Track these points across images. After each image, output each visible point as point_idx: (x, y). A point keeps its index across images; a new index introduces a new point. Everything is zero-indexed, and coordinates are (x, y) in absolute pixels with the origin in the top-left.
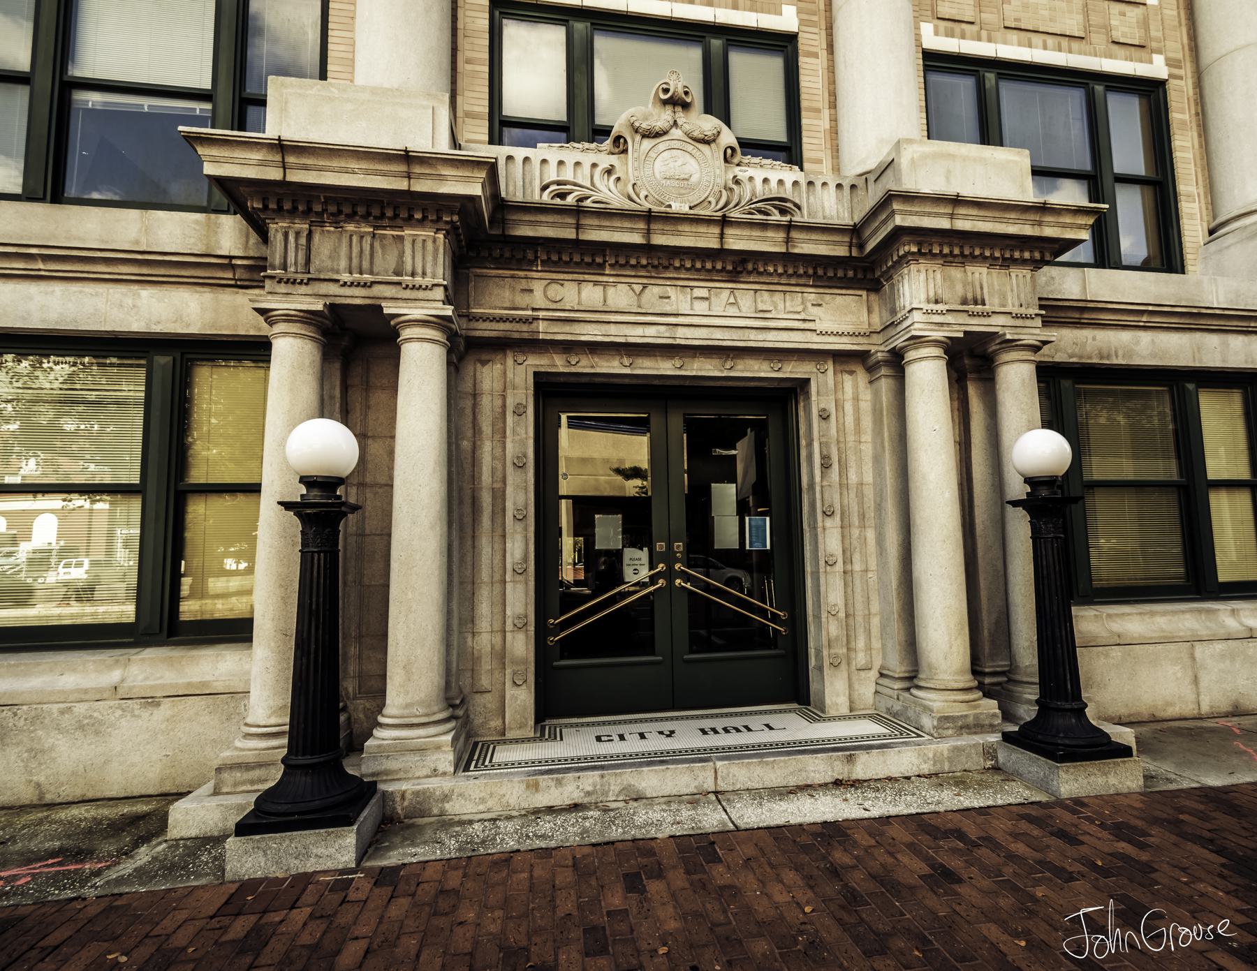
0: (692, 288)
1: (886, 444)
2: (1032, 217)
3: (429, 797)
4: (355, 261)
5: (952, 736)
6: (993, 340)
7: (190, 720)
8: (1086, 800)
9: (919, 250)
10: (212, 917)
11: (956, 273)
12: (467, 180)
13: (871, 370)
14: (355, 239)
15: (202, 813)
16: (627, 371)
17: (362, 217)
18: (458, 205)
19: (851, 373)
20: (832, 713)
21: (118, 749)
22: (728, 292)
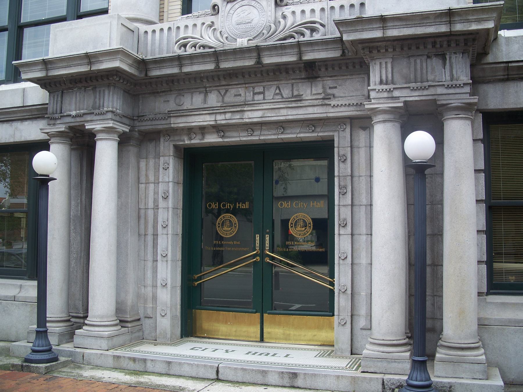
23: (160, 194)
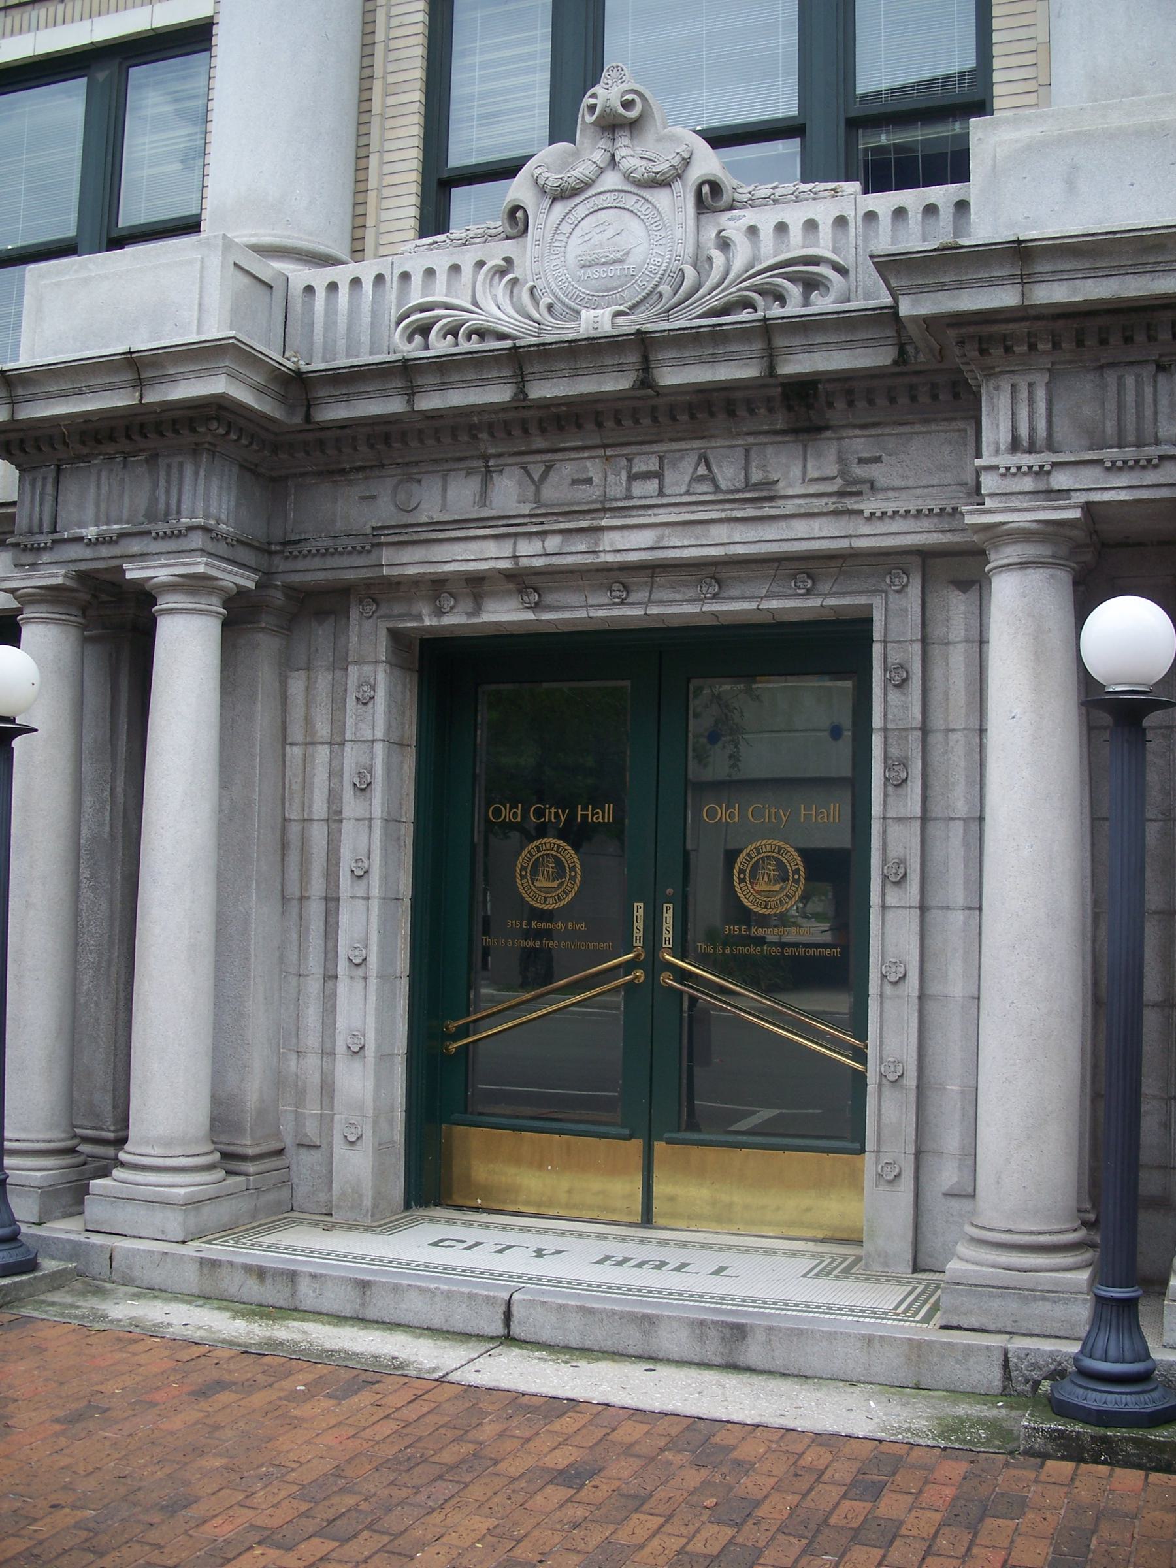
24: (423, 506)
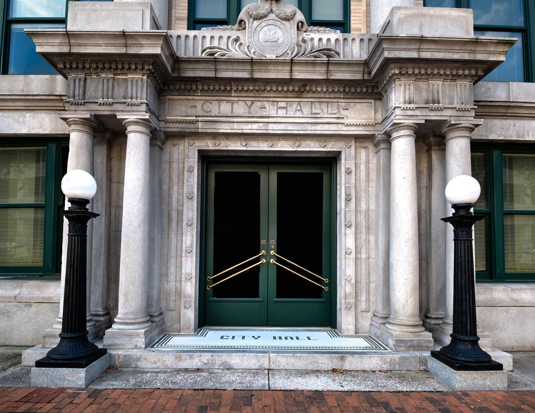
0: (277, 102)
1: (381, 187)
2: (469, 48)
3: (131, 358)
4: (105, 92)
5: (403, 351)
6: (445, 125)
7: (44, 314)
8: (469, 393)
9: (400, 72)
10: (16, 402)
11: (423, 85)
12: (153, 46)
13: (376, 145)
14: (105, 81)
15: (35, 355)
16: (244, 148)
17: (108, 69)
18: (152, 60)
19: (365, 148)
20: (346, 333)
21: (16, 324)
22: (297, 103)
23: (185, 194)
24: (212, 111)
